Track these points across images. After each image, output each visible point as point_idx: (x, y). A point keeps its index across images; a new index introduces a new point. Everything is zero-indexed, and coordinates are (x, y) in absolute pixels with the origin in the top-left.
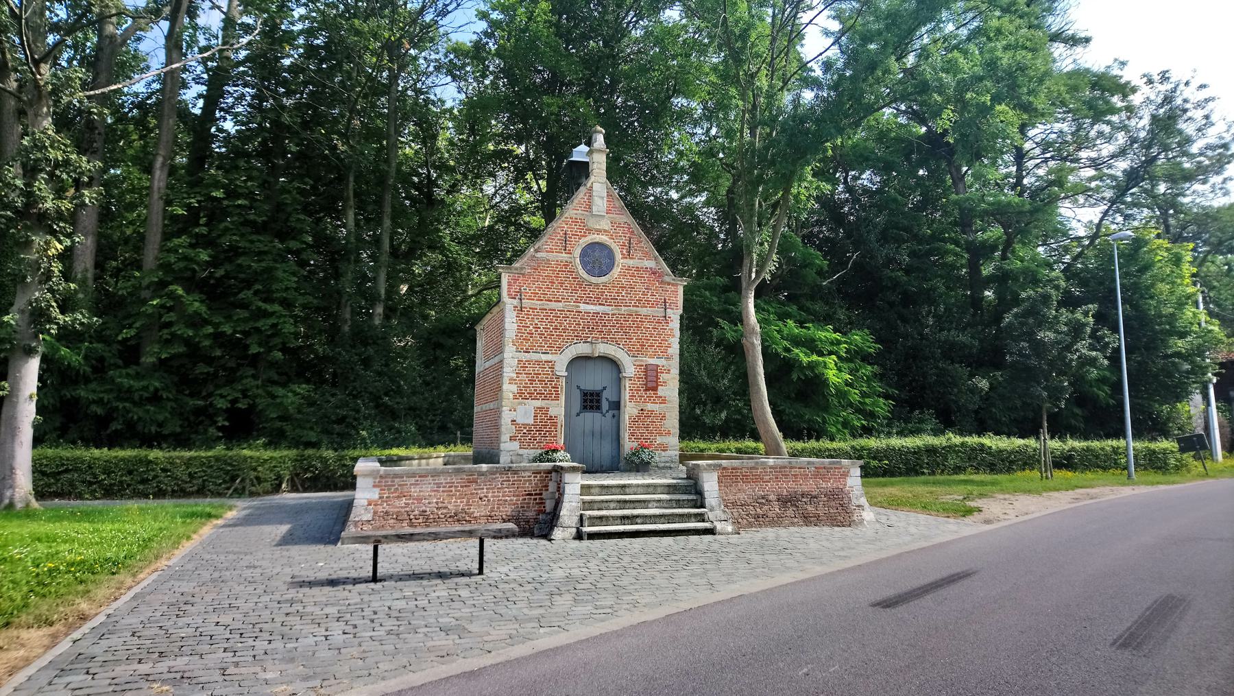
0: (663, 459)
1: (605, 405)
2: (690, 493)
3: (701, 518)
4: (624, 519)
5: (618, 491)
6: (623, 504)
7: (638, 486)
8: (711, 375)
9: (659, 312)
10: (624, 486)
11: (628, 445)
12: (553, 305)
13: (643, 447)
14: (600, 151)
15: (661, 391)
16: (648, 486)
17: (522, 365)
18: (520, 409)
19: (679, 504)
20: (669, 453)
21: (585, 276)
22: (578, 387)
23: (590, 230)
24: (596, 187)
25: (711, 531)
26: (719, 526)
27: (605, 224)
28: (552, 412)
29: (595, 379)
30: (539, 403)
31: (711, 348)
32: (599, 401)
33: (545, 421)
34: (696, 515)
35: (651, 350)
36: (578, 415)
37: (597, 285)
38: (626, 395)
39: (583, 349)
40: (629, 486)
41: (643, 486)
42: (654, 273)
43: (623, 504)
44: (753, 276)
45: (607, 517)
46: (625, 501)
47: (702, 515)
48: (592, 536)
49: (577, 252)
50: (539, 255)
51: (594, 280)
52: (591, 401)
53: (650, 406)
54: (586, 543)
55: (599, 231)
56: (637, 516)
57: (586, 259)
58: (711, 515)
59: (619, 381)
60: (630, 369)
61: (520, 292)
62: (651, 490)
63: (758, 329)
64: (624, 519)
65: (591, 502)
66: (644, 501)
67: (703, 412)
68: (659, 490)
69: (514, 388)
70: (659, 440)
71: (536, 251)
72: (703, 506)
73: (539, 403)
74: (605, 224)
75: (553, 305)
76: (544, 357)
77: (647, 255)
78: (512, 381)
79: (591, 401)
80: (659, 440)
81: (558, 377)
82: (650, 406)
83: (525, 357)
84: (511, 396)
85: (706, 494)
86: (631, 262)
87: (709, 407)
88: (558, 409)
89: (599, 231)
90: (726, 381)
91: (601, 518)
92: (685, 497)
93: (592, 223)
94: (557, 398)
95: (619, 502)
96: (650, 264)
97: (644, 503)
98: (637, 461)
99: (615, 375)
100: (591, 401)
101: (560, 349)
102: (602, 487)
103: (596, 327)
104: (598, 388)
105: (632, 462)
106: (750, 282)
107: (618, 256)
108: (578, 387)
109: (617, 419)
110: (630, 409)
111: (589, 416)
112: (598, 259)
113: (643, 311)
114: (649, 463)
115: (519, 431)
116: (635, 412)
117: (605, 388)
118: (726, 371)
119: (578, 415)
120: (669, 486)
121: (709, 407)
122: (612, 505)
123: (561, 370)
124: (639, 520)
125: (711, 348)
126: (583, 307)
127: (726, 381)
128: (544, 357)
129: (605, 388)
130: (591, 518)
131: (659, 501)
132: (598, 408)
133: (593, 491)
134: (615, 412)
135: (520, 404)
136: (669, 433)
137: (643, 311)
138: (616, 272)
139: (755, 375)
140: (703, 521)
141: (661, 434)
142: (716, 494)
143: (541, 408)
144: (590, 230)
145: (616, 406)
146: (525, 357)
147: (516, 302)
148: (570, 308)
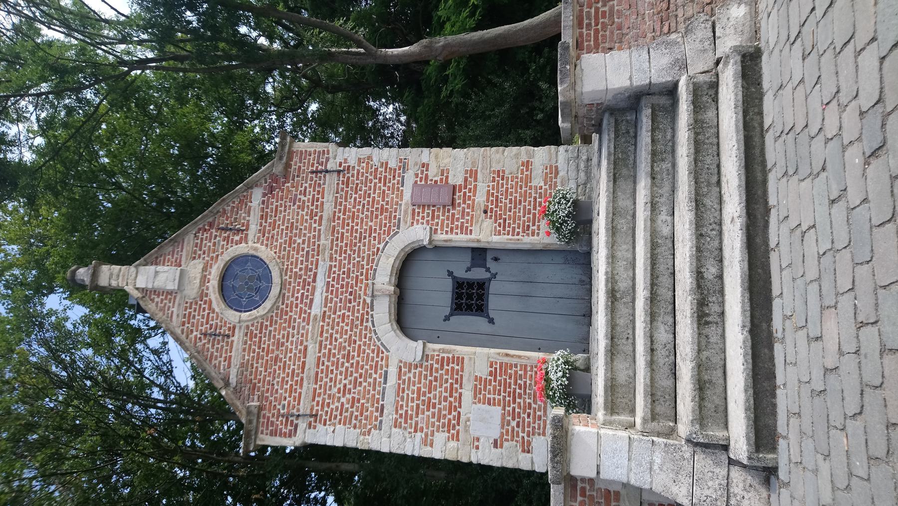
0: (572, 174)
1: (478, 274)
2: (636, 124)
3: (706, 94)
4: (707, 315)
5: (622, 310)
6: (661, 304)
7: (612, 258)
8: (500, 103)
9: (331, 181)
10: (613, 295)
11: (542, 236)
12: (311, 360)
13: (545, 213)
14: (95, 275)
15: (456, 179)
16: (613, 231)
17: (403, 420)
18: (476, 429)
19: (663, 152)
20: (561, 163)
21: (268, 304)
22: (447, 318)
23: (202, 295)
24: (141, 283)
25: (750, 61)
26: (729, 42)
27: (195, 269)
28: (483, 371)
29: (434, 291)
30: (467, 394)
31: (471, 104)
32: (470, 284)
33: (499, 386)
34: (697, 106)
35: (391, 196)
36: (491, 321)
37: (283, 285)
38: (460, 239)
39: (383, 311)
40: (612, 279)
41: (612, 245)
42: (272, 189)
43: (661, 304)
44: (362, 50)
45: (701, 367)
46: (653, 299)
47: (696, 91)
48: (764, 434)
49: (232, 316)
50: (233, 380)
51: (275, 291)
52: (470, 297)
53: (480, 198)
54: (785, 454)
55: (204, 279)
56: (699, 275)
57: (244, 301)
58: (699, 66)
59: (438, 249)
60: (416, 233)
61: (287, 416)
62: (623, 224)
63: (424, 41)
64: (707, 315)
65: (653, 396)
66: (654, 246)
67: (542, 111)
68: (623, 203)
69: (440, 438)
70: (538, 181)
71: (227, 384)
72: (671, 91)
73: (467, 394)
74: (195, 269)
75: (311, 360)
76: (392, 380)
77: (244, 202)
78: (427, 442)
79: (470, 297)
80: (538, 181)
81: (425, 357)
82: (480, 198)
83: (389, 414)
84: (452, 444)
85: (640, 80)
86: (253, 228)
87: (537, 104)
88: (478, 359)
89: (204, 279)
90: (507, 85)
91: (701, 386)
92: (645, 138)
93: (192, 291)
94: (460, 361)
95: (652, 317)
96: (257, 195)
97: (661, 248)
98: (571, 225)
99: (430, 256)
100: (470, 298)
101: (381, 350)
102: (612, 352)
103: (348, 289)
104: (449, 284)
105: (572, 233)
106: (368, 53)
107: (242, 249)
108: (447, 318)
109: (499, 254)
110: (484, 233)
111: (494, 303)
112: (243, 283)
113: (329, 208)
114: (576, 203)
115: (514, 435)
116: (488, 224)
117: (450, 274)
118: (495, 85)
119: (491, 321)
120: (615, 178)
121: (537, 104)
122: (663, 335)
123: (412, 350)
124: (711, 271)
125: (471, 104)
126: (316, 310)
127: (507, 85)
128: (392, 380)
129: (450, 274)
130: (701, 418)
131: (654, 206)
132: (482, 286)
133: (622, 378)
134: (489, 257)
135: (467, 430)
136: (527, 164)
137: (329, 208)
138: (265, 253)
139: (484, 41)
140: (715, 86)
141: (529, 179)
142: (639, 56)
143: (476, 392)
144: (202, 295)
145: (479, 254)
146: (389, 414)
147: (302, 425)
148: (318, 330)
